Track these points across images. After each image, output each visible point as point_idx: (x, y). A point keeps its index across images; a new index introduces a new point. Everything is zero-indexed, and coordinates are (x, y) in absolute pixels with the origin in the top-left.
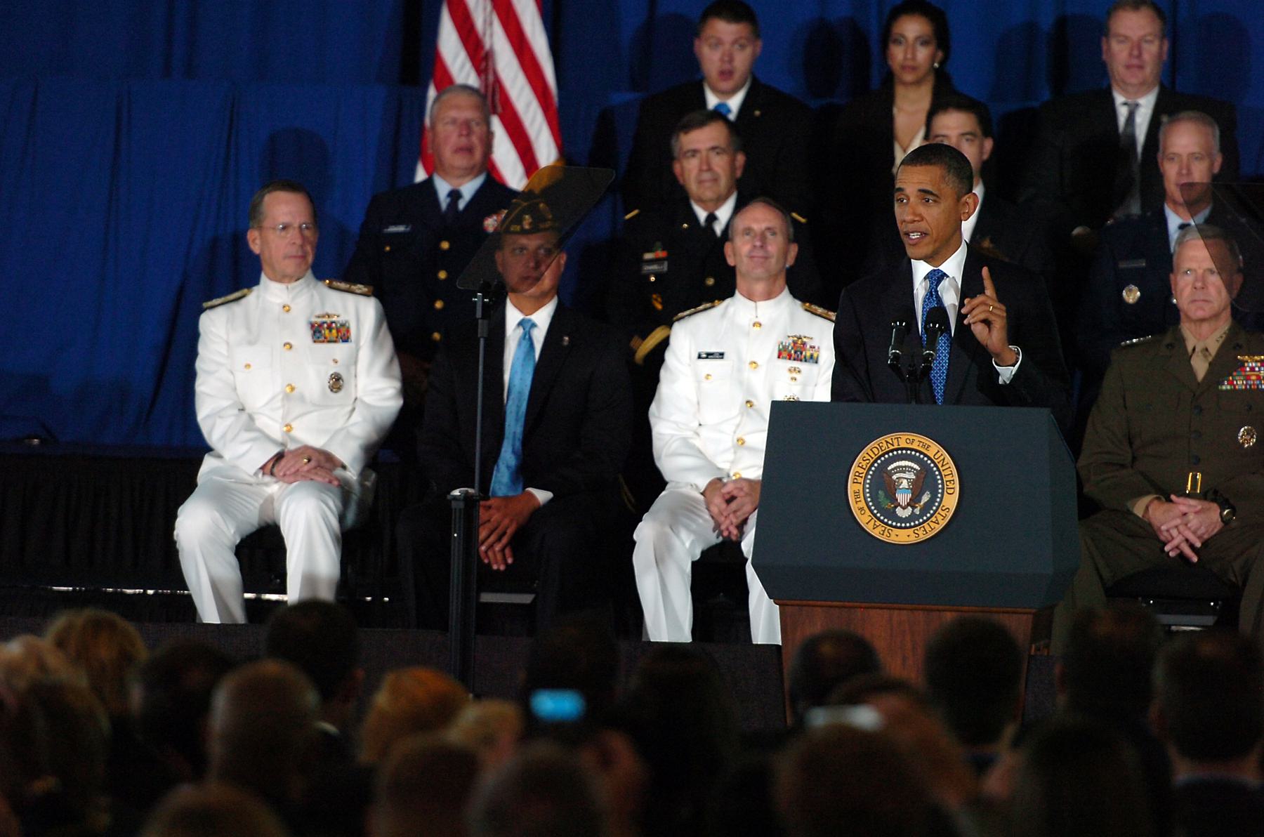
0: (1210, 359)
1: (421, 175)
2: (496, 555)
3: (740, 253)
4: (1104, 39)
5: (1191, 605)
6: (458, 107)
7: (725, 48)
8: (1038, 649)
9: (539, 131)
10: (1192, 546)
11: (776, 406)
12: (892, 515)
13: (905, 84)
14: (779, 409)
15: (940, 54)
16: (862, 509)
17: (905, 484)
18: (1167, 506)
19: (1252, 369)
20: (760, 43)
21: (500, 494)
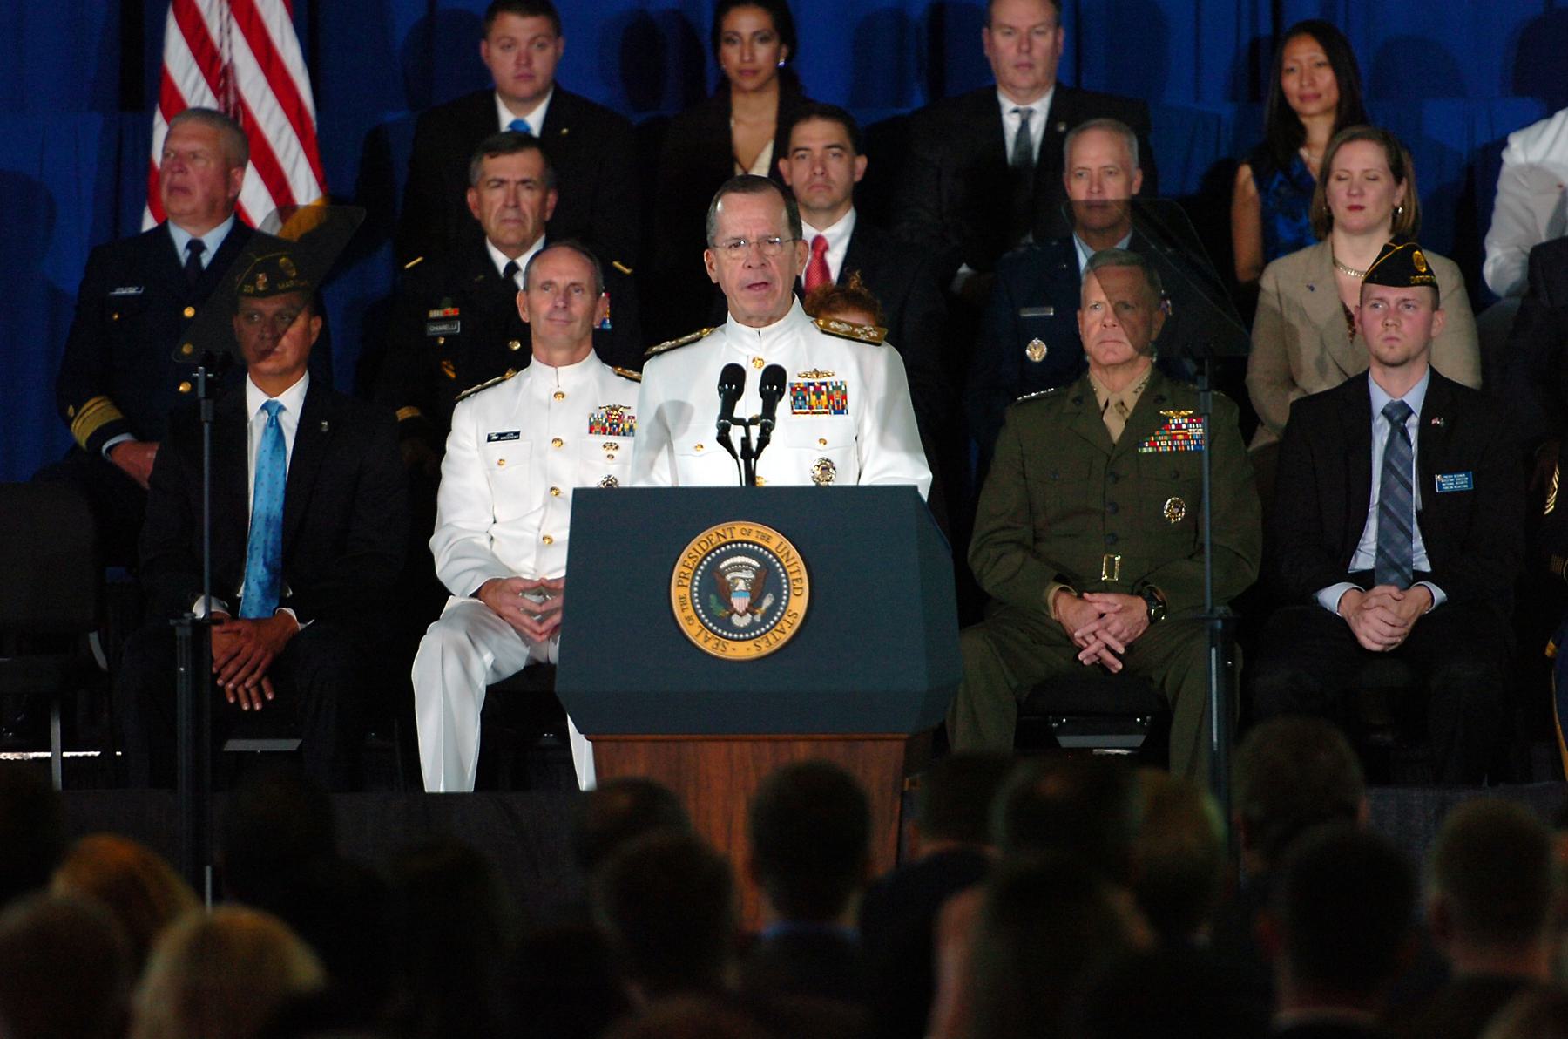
0: (1127, 415)
1: (149, 223)
2: (245, 690)
3: (537, 308)
4: (985, 30)
5: (1117, 722)
7: (519, 49)
8: (913, 783)
9: (296, 163)
10: (1113, 652)
11: (576, 491)
12: (726, 624)
13: (744, 92)
14: (584, 500)
15: (785, 50)
16: (689, 618)
17: (741, 585)
18: (1079, 603)
19: (1179, 427)
20: (561, 42)
21: (252, 616)
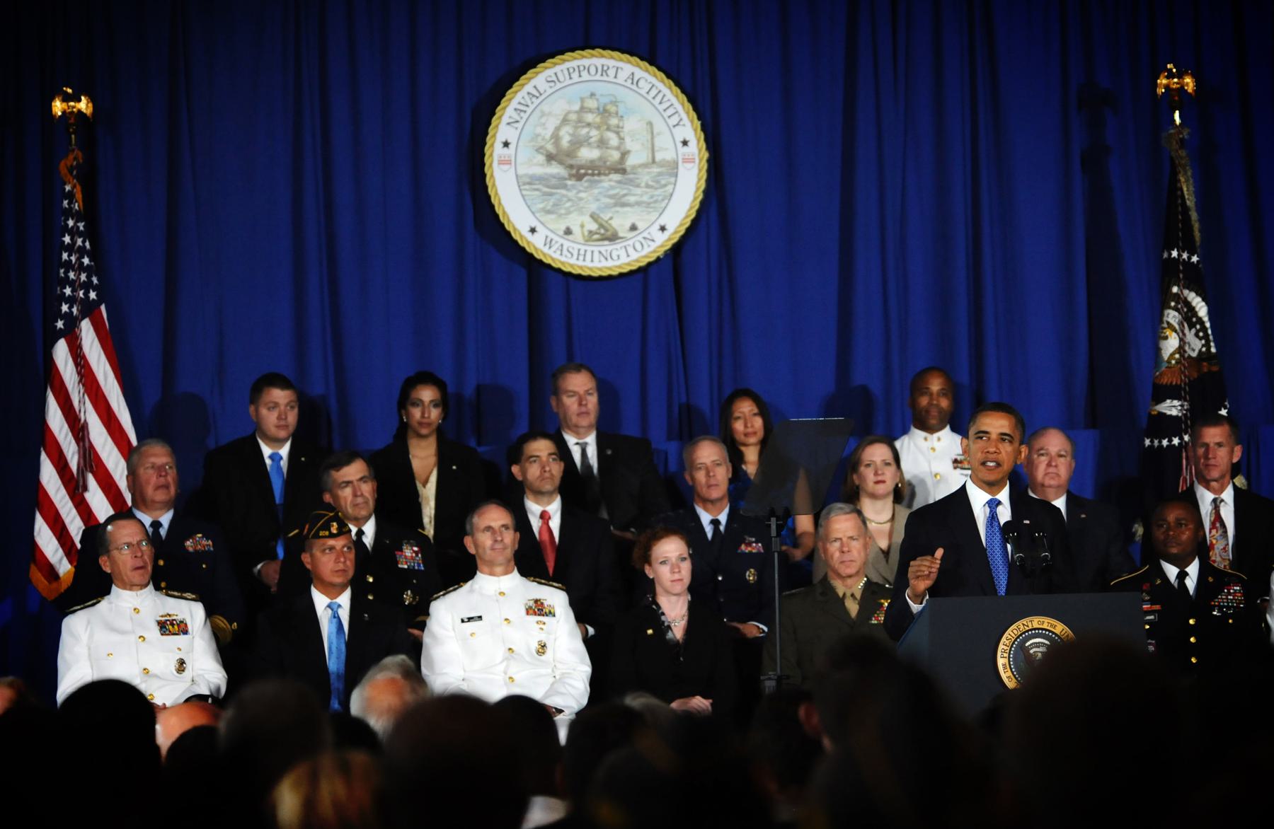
6: (155, 455)
